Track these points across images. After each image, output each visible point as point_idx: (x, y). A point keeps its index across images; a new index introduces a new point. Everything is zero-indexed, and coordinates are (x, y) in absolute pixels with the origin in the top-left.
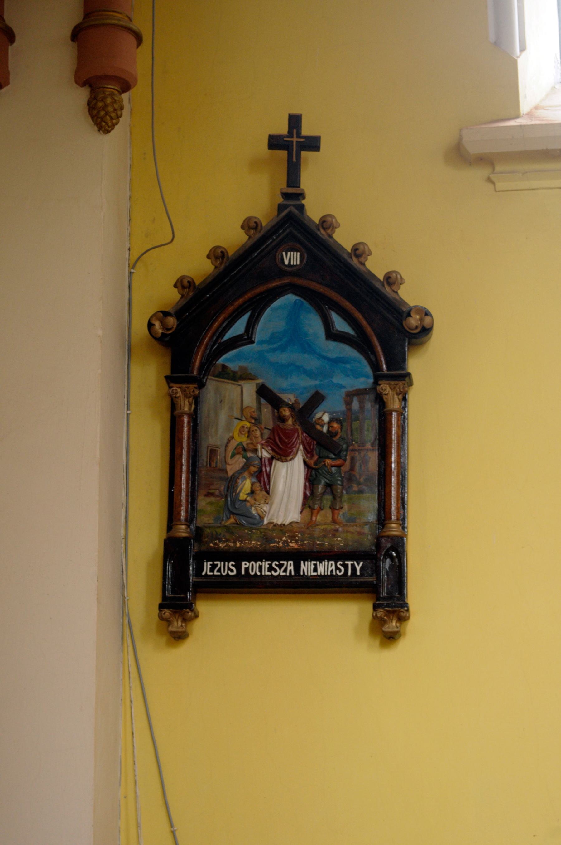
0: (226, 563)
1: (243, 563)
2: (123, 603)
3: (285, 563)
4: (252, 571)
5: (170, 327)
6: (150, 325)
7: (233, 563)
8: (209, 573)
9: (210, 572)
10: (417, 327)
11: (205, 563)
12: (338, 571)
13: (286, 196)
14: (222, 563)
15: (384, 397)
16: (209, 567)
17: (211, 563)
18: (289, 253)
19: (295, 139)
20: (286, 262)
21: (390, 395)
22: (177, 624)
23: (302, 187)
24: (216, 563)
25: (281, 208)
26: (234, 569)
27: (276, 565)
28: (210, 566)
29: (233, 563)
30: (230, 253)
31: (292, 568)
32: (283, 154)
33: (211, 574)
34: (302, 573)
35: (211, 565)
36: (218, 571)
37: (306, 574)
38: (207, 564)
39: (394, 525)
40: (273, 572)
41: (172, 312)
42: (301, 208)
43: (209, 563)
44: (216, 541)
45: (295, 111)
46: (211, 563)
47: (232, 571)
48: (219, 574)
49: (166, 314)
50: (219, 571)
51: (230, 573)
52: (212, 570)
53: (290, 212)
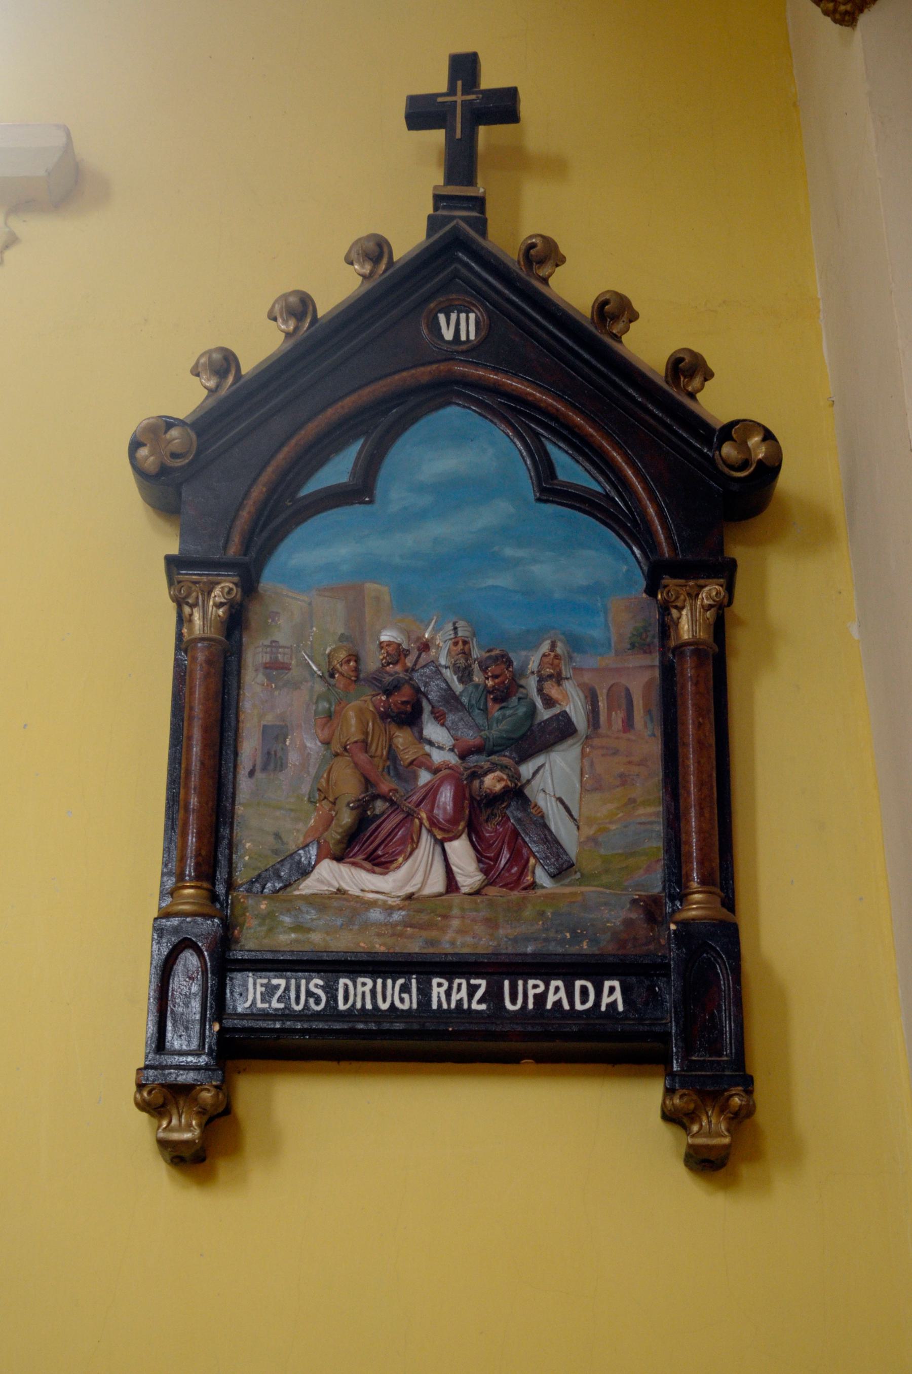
0: (389, 982)
1: (435, 981)
2: (426, 882)
3: (282, 982)
4: (298, 1003)
5: (179, 450)
6: (135, 445)
7: (321, 983)
9: (263, 1001)
10: (745, 464)
11: (251, 980)
12: (311, 1001)
13: (439, 199)
14: (379, 981)
15: (674, 612)
16: (260, 989)
17: (265, 981)
18: (454, 316)
20: (448, 335)
21: (580, 699)
22: (180, 1121)
24: (275, 982)
25: (433, 223)
26: (320, 992)
27: (316, 986)
28: (263, 989)
30: (323, 309)
31: (562, 994)
32: (437, 136)
34: (435, 1006)
37: (445, 1006)
38: (255, 984)
39: (697, 897)
41: (188, 421)
42: (481, 225)
43: (259, 981)
44: (689, 557)
45: (525, 108)
46: (265, 981)
49: (170, 423)
53: (454, 227)
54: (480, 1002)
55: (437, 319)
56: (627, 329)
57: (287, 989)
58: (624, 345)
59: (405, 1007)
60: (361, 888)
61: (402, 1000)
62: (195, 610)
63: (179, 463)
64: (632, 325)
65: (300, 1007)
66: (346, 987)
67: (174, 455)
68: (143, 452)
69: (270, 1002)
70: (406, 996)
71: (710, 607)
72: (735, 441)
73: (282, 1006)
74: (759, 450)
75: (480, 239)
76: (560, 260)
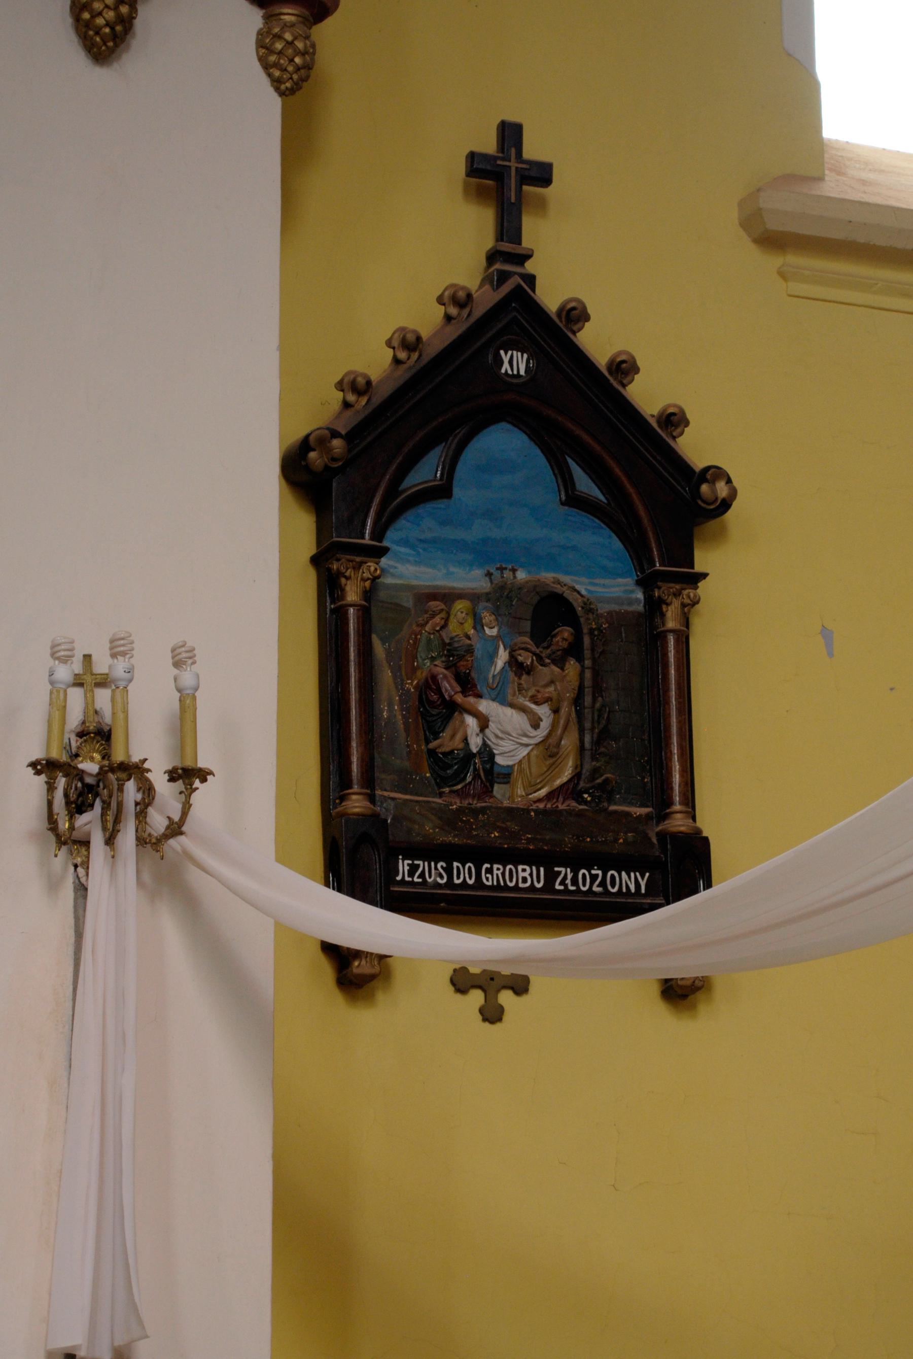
7: (444, 865)
8: (407, 879)
11: (400, 861)
14: (426, 864)
15: (664, 607)
16: (407, 868)
17: (410, 862)
19: (513, 164)
23: (525, 243)
24: (416, 862)
29: (444, 865)
33: (410, 879)
35: (408, 865)
36: (419, 877)
40: (439, 880)
43: (406, 862)
46: (410, 862)
47: (441, 877)
48: (420, 880)
50: (422, 875)
51: (439, 880)
52: (411, 873)
54: (560, 873)
55: (500, 354)
56: (682, 434)
57: (565, 877)
58: (678, 444)
59: (490, 883)
60: (168, 815)
61: (487, 879)
62: (349, 582)
63: (335, 465)
64: (686, 429)
65: (508, 867)
66: (613, 876)
67: (334, 460)
68: (312, 455)
69: (413, 878)
70: (489, 876)
71: (368, 579)
72: (709, 483)
73: (420, 880)
74: (722, 489)
75: (532, 294)
76: (687, 423)
